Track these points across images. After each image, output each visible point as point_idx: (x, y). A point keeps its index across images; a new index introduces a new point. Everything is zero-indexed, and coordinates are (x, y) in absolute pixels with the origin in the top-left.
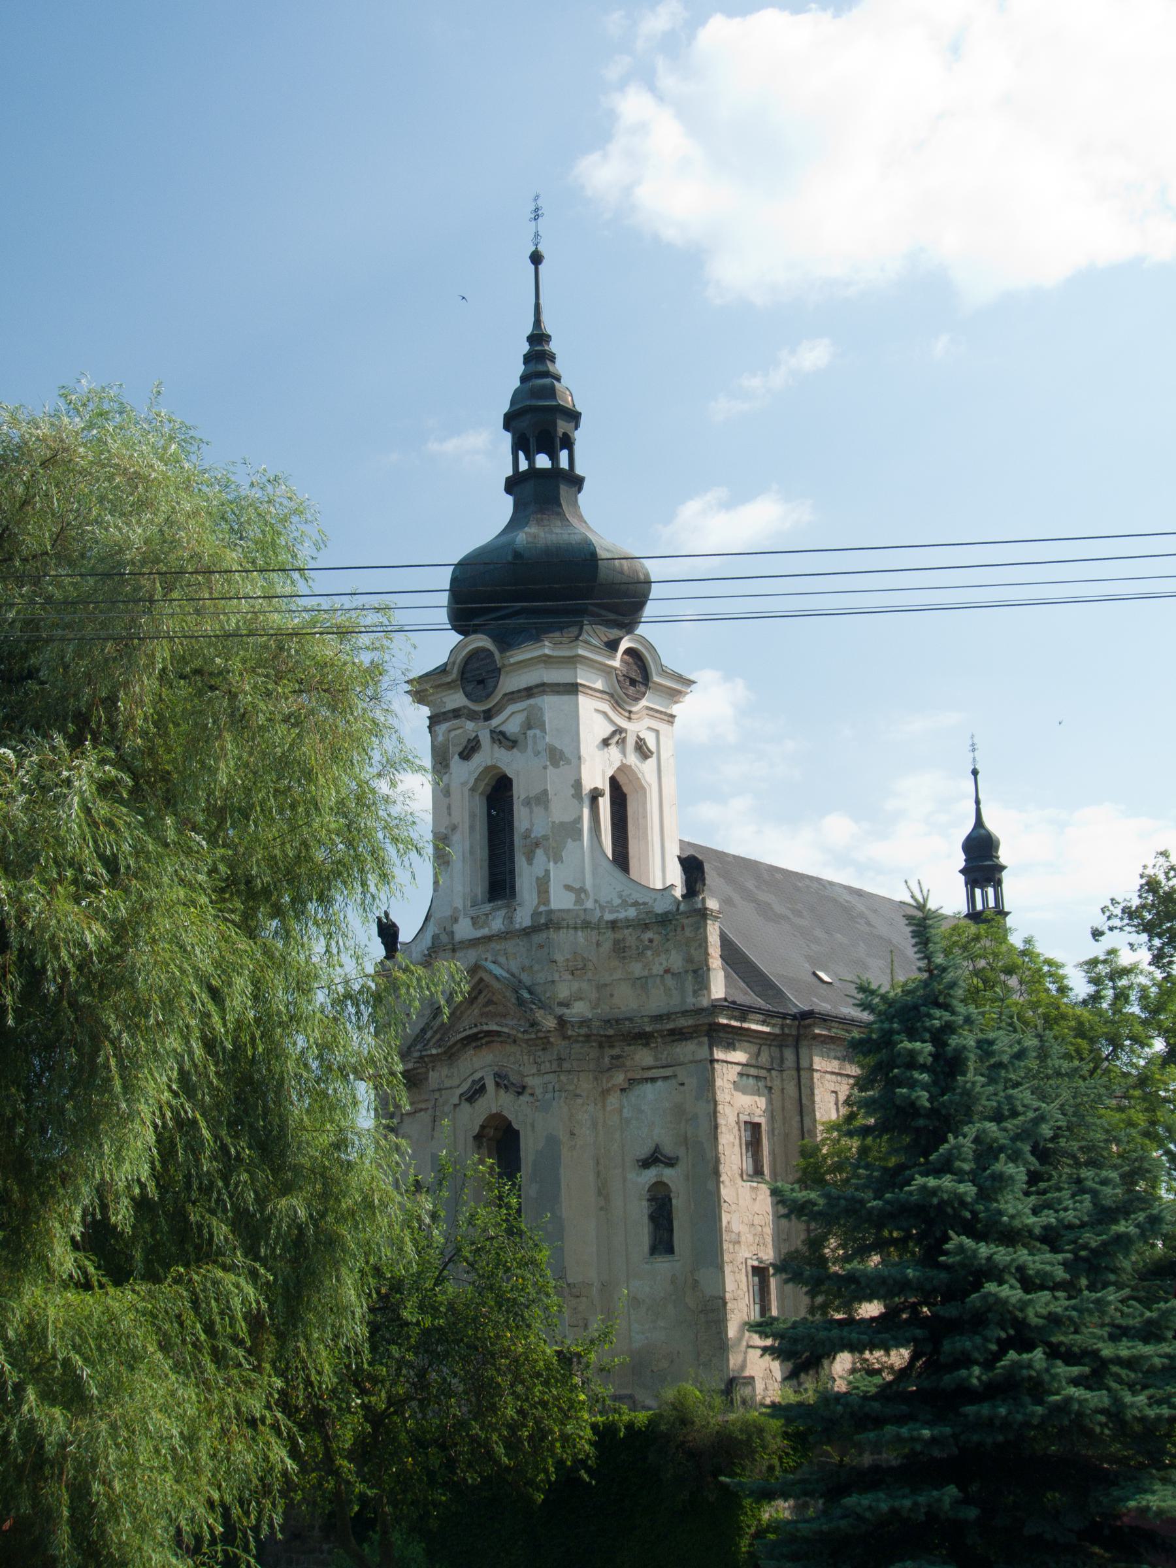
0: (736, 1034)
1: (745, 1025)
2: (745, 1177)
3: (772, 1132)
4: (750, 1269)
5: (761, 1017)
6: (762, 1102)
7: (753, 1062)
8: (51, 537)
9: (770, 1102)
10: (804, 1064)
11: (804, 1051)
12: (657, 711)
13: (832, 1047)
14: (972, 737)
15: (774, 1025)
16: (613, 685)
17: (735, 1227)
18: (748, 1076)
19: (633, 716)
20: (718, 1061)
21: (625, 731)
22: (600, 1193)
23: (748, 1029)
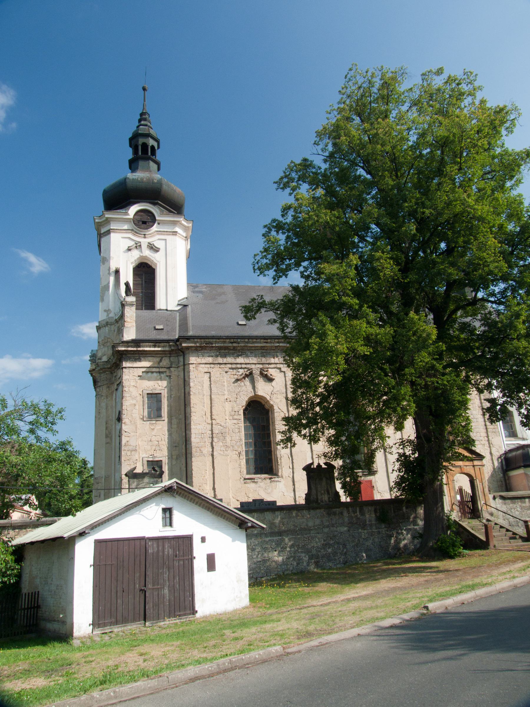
0: (142, 354)
1: (139, 349)
2: (145, 419)
3: (170, 397)
4: (146, 463)
5: (151, 344)
6: (164, 383)
7: (156, 366)
8: (380, 326)
9: (169, 383)
10: (186, 362)
11: (186, 356)
12: (164, 231)
13: (206, 351)
14: (143, 116)
15: (163, 347)
16: (133, 226)
17: (133, 442)
18: (152, 372)
19: (146, 236)
20: (125, 368)
21: (140, 242)
22: (107, 436)
23: (144, 351)
